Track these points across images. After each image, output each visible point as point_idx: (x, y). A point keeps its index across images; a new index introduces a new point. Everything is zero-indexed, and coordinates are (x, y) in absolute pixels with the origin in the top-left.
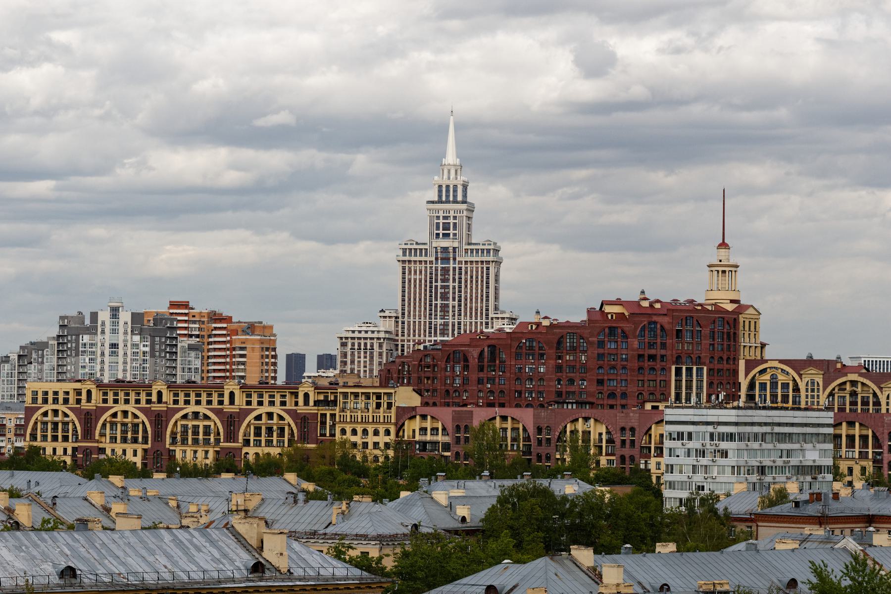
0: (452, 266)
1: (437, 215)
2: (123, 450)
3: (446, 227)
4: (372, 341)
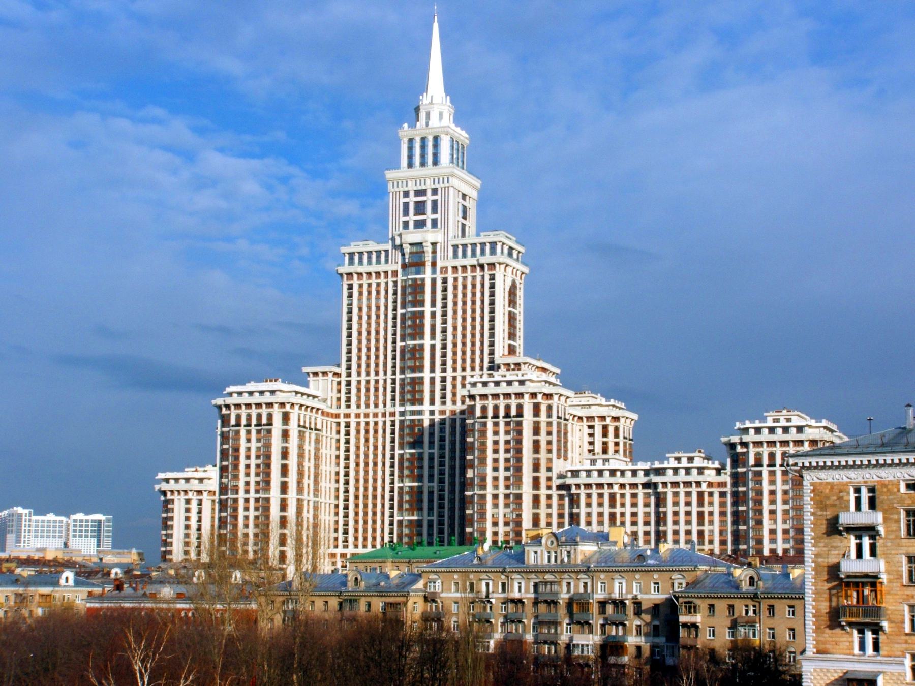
3: (420, 208)
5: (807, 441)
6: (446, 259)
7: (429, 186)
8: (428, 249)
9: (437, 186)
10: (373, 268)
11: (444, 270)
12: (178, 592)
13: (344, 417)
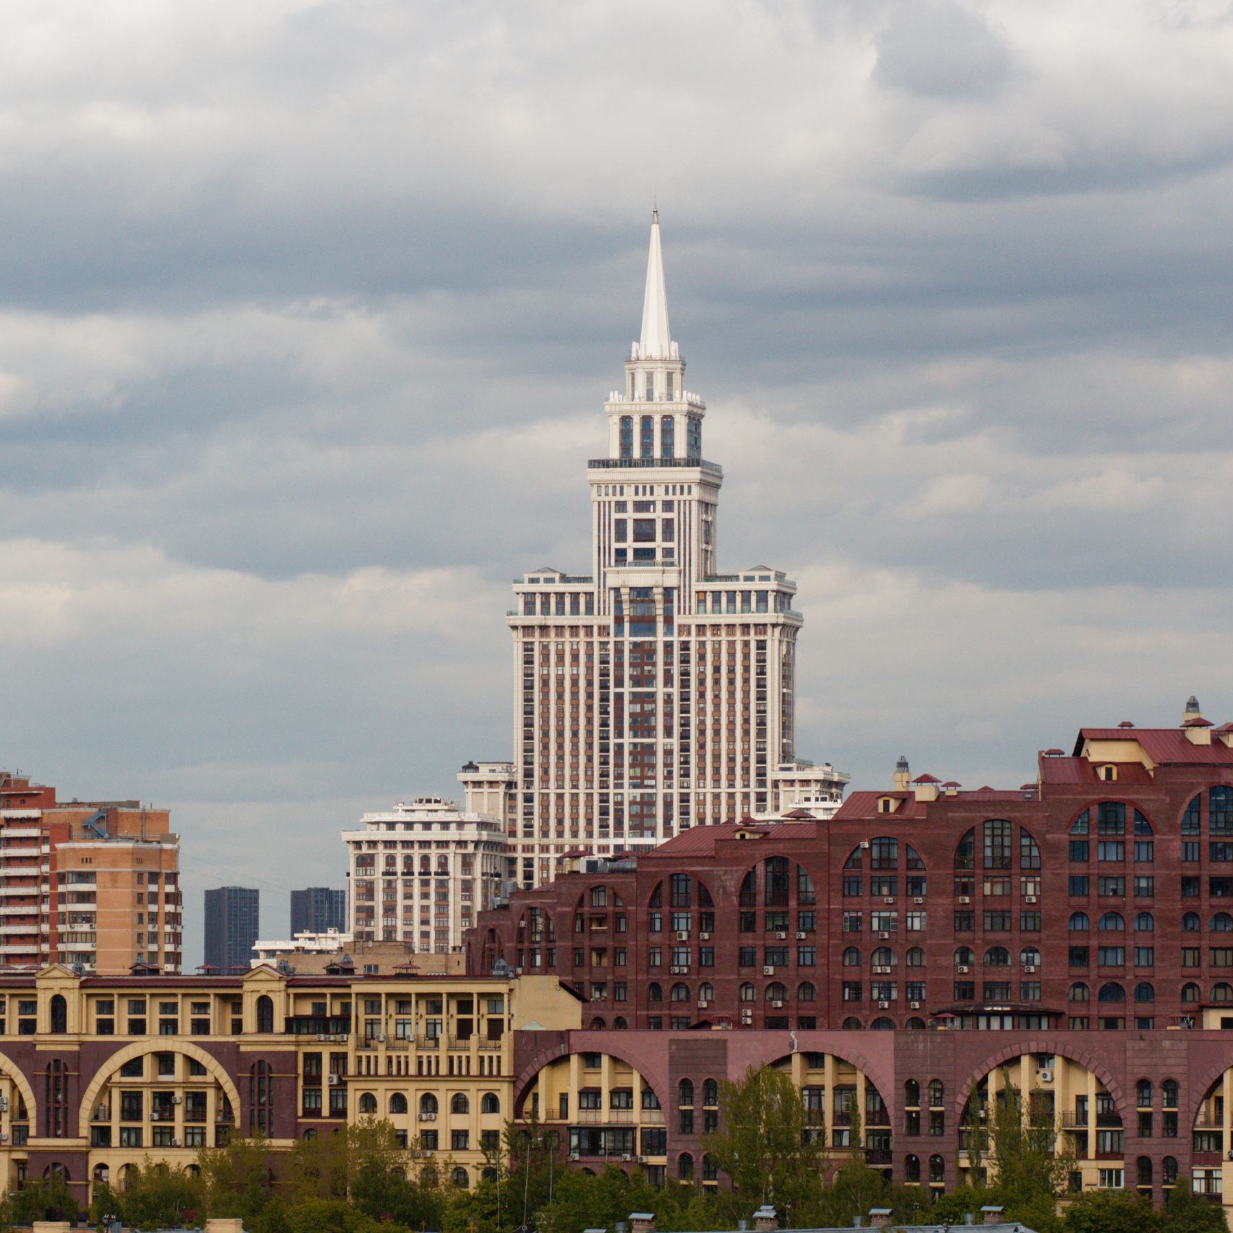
1: (618, 498)
3: (644, 531)
4: (392, 851)
5: (177, 888)
6: (687, 612)
7: (659, 495)
8: (658, 595)
9: (670, 497)
10: (567, 620)
11: (684, 629)
13: (524, 851)
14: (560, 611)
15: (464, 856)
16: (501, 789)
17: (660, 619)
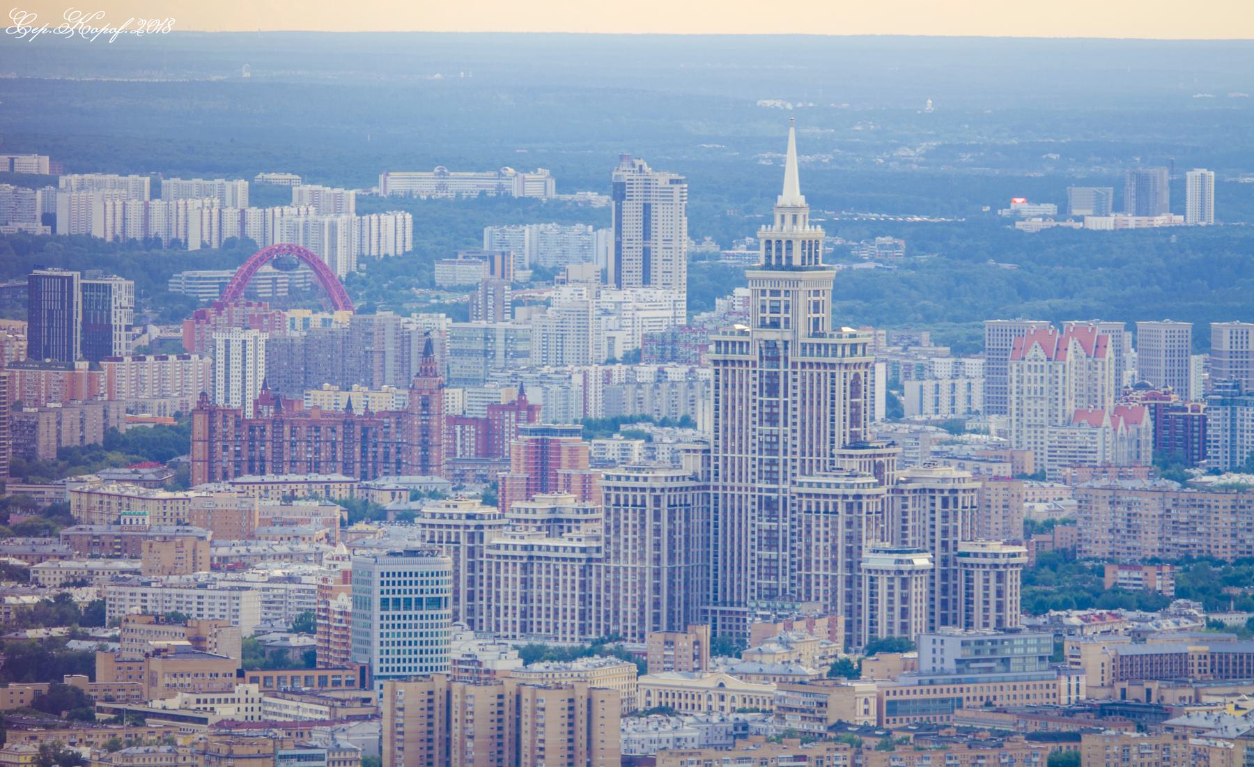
0: (782, 369)
1: (762, 288)
2: (528, 352)
11: (794, 365)
12: (959, 657)
14: (826, 355)
15: (847, 503)
16: (700, 455)
17: (782, 359)
